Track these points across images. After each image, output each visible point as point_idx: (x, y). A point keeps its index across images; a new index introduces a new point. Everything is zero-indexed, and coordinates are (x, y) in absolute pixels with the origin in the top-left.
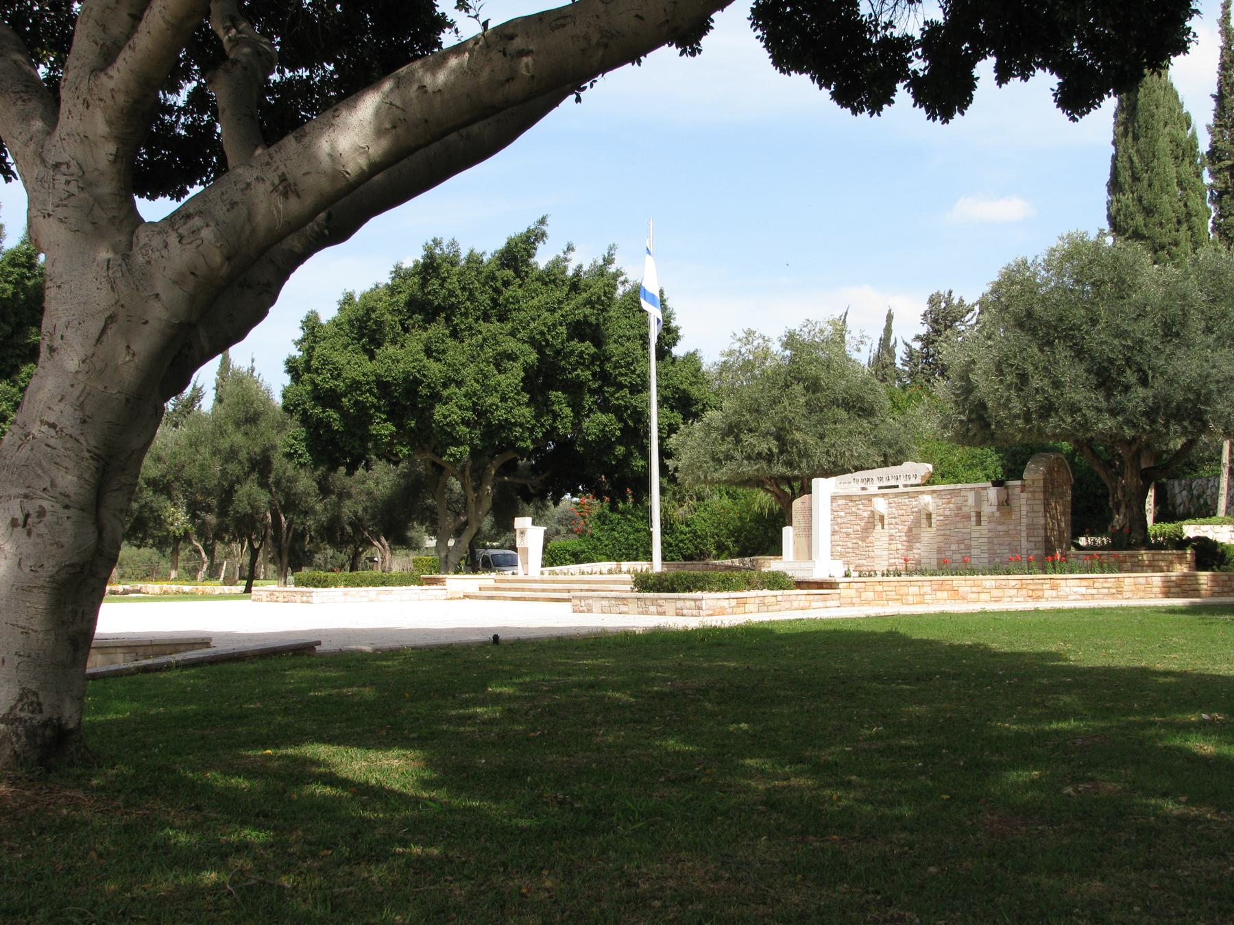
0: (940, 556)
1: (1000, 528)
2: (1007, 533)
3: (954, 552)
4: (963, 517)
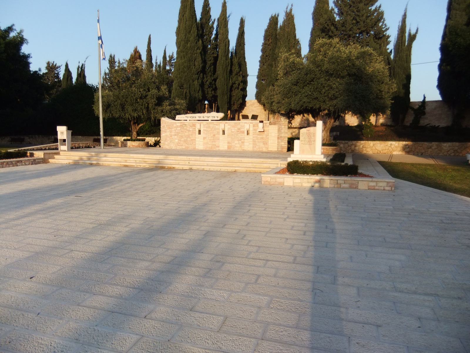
0: (229, 145)
1: (258, 136)
2: (262, 138)
3: (236, 144)
4: (241, 132)
